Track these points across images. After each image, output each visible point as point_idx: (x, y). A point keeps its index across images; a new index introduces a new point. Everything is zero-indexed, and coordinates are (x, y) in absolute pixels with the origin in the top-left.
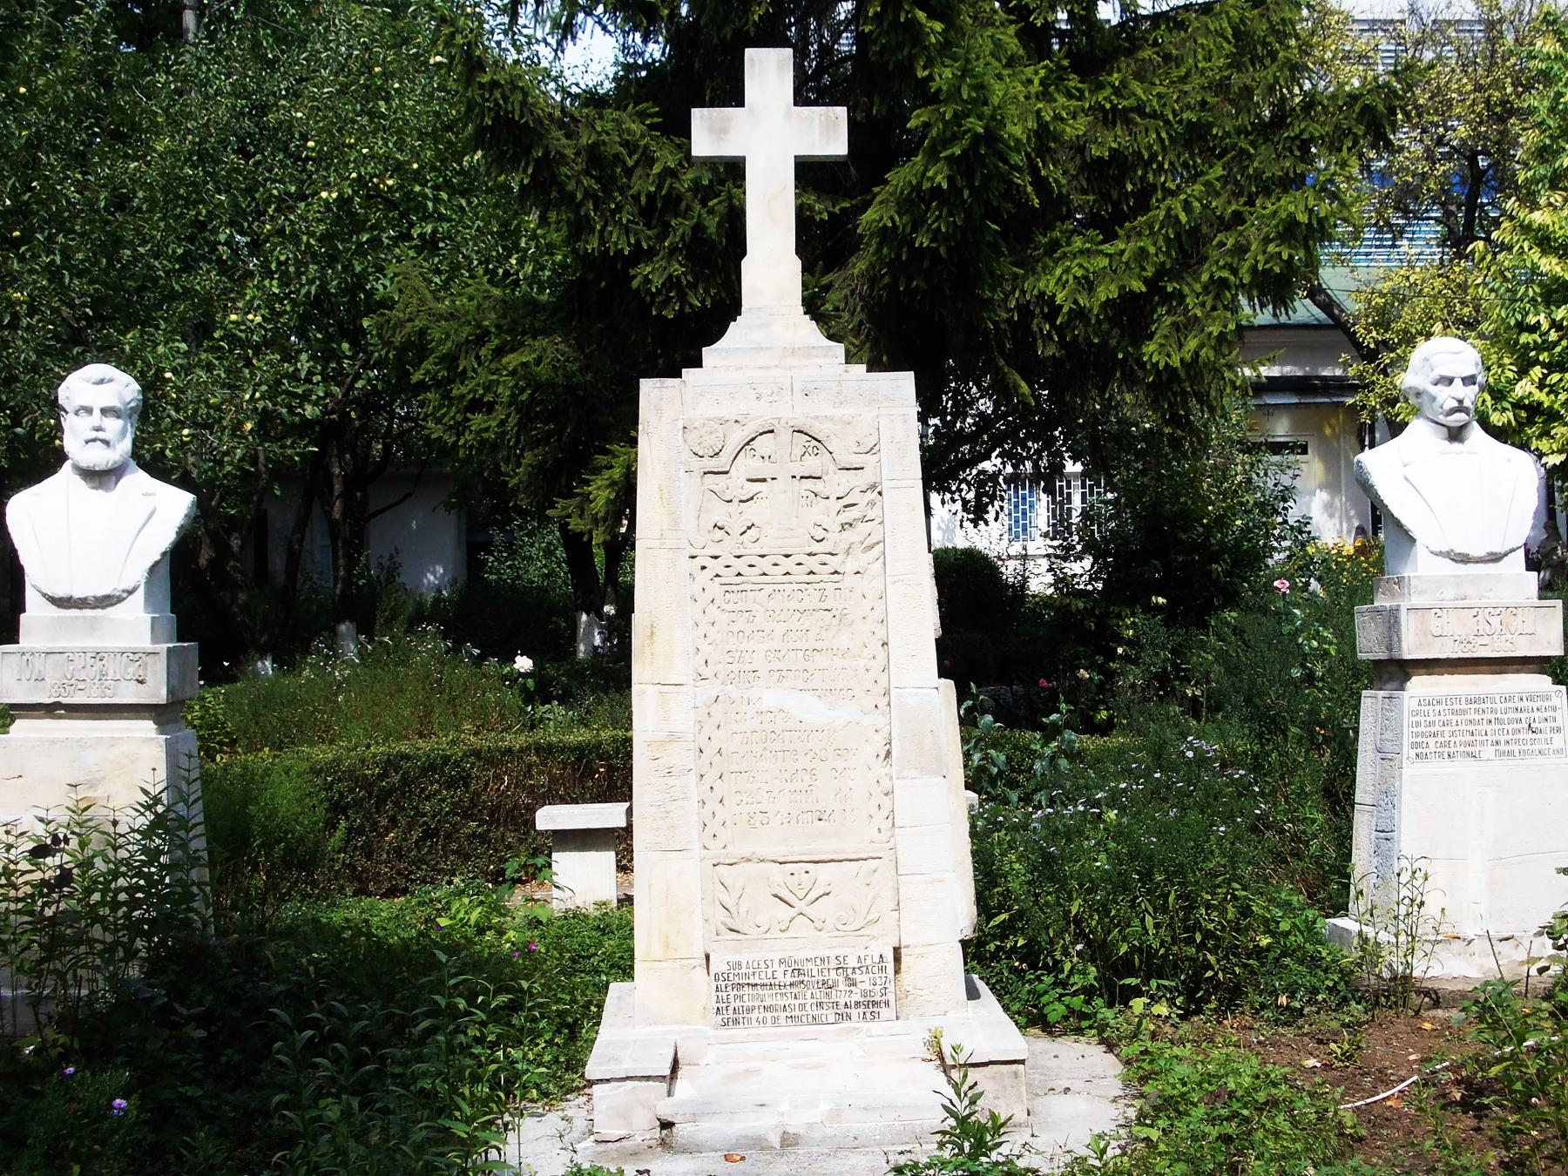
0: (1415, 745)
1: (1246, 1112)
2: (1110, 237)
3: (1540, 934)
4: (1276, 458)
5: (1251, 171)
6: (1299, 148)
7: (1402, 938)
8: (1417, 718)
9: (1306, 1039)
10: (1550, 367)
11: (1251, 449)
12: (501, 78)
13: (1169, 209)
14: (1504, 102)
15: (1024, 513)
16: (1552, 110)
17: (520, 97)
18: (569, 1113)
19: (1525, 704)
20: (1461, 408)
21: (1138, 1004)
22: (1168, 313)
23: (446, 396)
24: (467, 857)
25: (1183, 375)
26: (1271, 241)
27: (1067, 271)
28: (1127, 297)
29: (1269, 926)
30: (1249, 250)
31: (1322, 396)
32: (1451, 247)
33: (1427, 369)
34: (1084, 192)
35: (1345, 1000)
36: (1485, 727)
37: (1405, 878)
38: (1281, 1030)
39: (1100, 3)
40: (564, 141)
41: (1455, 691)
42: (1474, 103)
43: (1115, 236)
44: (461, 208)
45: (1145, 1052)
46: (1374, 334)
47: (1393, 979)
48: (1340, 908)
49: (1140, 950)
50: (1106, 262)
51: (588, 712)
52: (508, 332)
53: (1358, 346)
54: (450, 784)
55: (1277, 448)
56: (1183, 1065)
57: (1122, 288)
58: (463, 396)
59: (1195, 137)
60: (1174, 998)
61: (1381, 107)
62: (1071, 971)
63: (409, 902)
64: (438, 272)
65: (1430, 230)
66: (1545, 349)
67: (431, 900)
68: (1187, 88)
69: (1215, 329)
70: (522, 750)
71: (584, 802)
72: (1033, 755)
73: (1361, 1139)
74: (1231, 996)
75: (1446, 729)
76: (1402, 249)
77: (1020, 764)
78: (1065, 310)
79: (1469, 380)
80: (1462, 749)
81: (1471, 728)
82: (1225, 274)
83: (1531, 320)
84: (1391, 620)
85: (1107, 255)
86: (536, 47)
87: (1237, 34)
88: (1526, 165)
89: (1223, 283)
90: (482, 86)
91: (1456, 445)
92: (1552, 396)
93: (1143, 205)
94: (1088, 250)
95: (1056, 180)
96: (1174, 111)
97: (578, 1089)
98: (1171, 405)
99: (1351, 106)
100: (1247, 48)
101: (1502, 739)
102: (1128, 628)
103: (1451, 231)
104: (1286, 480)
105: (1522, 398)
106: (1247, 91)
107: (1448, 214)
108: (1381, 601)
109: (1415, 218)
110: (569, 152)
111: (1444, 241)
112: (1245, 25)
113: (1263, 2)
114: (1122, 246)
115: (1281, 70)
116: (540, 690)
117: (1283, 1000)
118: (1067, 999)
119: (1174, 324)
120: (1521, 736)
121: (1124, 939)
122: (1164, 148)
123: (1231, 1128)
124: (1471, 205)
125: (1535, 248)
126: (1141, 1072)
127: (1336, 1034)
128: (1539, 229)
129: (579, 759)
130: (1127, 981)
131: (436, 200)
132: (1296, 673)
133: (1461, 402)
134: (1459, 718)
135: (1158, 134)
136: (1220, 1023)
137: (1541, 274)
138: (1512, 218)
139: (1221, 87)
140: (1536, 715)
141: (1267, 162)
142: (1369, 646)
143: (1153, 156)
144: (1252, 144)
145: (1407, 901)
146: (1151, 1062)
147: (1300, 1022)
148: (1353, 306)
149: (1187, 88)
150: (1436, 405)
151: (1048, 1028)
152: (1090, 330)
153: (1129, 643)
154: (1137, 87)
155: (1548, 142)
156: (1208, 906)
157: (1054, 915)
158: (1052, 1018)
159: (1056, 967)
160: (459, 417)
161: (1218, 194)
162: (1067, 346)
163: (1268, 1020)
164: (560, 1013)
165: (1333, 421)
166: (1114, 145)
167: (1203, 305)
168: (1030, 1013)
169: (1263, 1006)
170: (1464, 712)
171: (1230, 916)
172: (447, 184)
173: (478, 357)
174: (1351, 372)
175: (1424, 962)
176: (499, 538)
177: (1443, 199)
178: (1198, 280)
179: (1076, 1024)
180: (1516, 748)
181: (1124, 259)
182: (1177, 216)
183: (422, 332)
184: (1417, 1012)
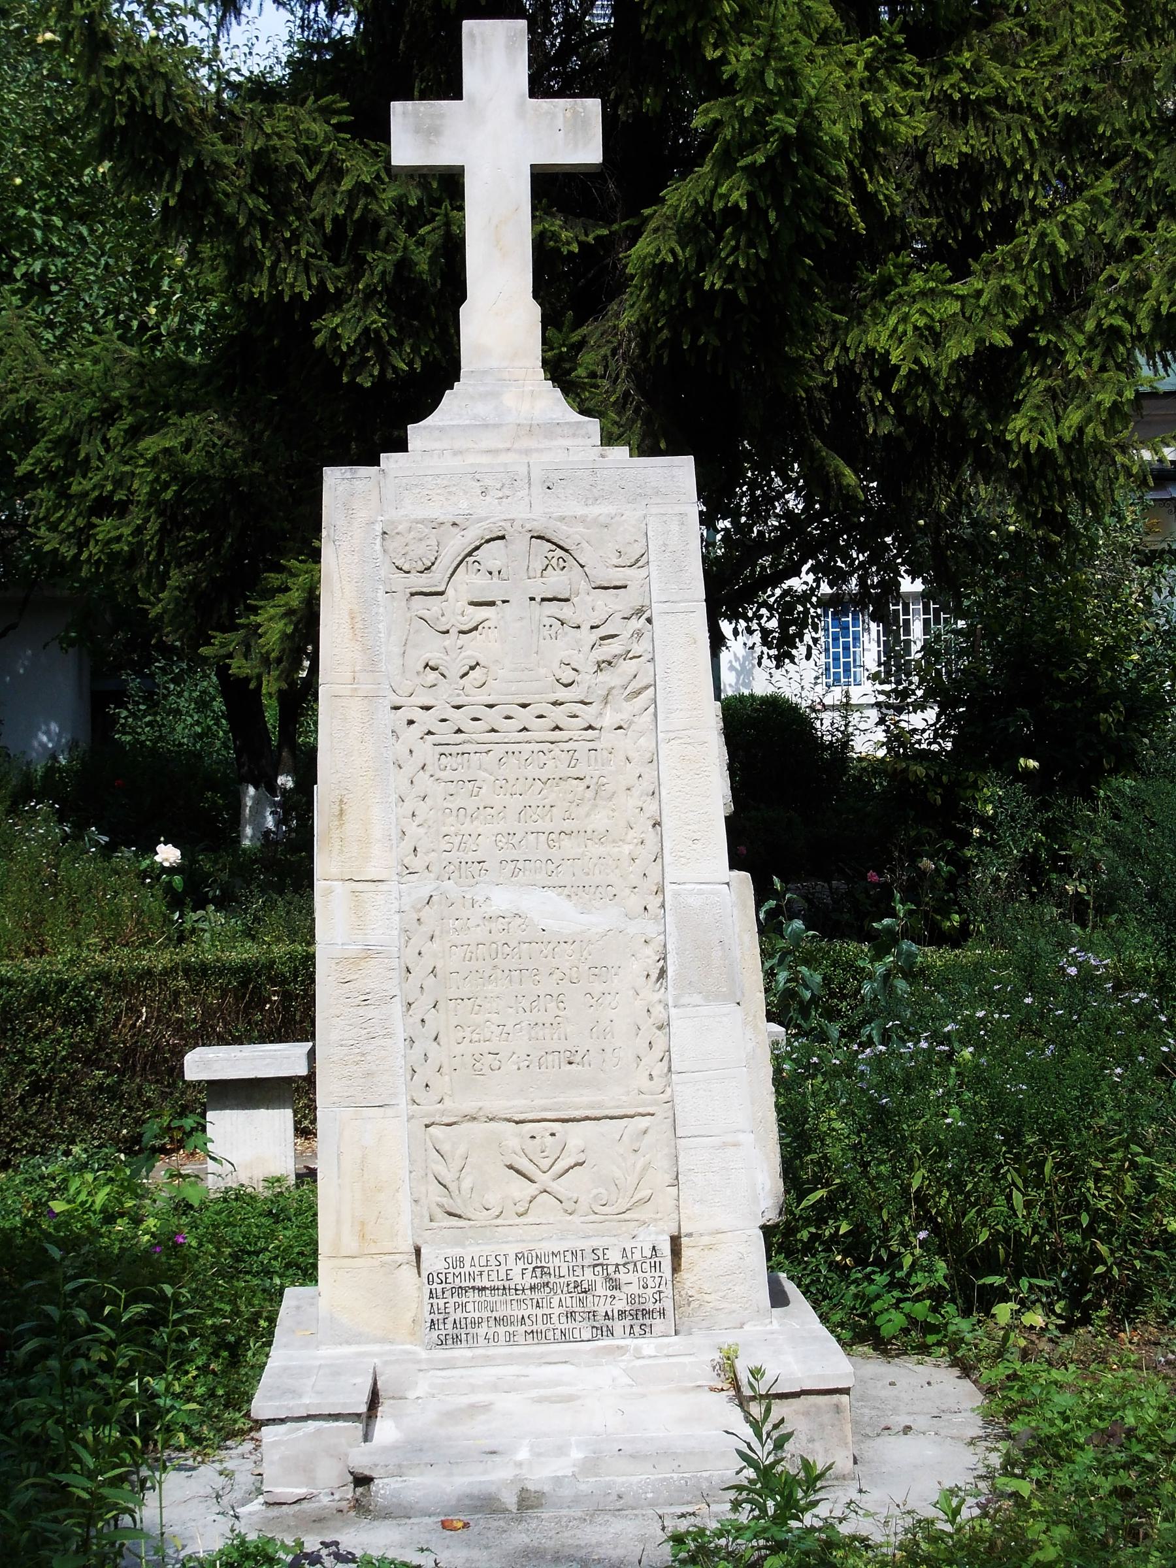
1: (1149, 1457)
2: (961, 273)
5: (1150, 183)
12: (136, 60)
13: (1043, 235)
15: (846, 648)
17: (162, 87)
18: (229, 1465)
21: (1003, 1311)
22: (1041, 374)
23: (63, 492)
24: (90, 1118)
27: (905, 319)
28: (987, 355)
34: (925, 213)
40: (221, 146)
44: (81, 237)
49: (1006, 1239)
50: (956, 307)
51: (257, 919)
52: (147, 405)
54: (68, 1019)
56: (1065, 1393)
57: (980, 341)
58: (85, 494)
59: (1075, 136)
60: (1052, 1304)
63: (10, 1179)
64: (50, 325)
67: (42, 1177)
68: (1061, 71)
69: (1106, 398)
70: (166, 972)
71: (251, 1041)
74: (1130, 1302)
78: (903, 371)
82: (1118, 321)
85: (958, 297)
86: (181, 20)
89: (1115, 333)
90: (109, 72)
94: (932, 290)
95: (887, 198)
96: (1045, 101)
97: (242, 1432)
102: (986, 801)
110: (229, 161)
114: (979, 285)
116: (190, 890)
118: (907, 1306)
119: (1049, 389)
122: (1032, 153)
123: (1129, 1479)
129: (244, 984)
131: (48, 227)
135: (1025, 135)
136: (1114, 1336)
139: (1107, 69)
144: (1150, 146)
146: (1021, 1390)
149: (1061, 71)
154: (995, 71)
156: (1098, 1177)
158: (887, 1331)
159: (894, 1261)
160: (81, 522)
164: (217, 1330)
167: (1088, 363)
168: (856, 1325)
171: (1129, 1190)
172: (62, 207)
173: (105, 440)
176: (134, 684)
178: (1080, 329)
179: (919, 1340)
181: (982, 302)
183: (30, 407)
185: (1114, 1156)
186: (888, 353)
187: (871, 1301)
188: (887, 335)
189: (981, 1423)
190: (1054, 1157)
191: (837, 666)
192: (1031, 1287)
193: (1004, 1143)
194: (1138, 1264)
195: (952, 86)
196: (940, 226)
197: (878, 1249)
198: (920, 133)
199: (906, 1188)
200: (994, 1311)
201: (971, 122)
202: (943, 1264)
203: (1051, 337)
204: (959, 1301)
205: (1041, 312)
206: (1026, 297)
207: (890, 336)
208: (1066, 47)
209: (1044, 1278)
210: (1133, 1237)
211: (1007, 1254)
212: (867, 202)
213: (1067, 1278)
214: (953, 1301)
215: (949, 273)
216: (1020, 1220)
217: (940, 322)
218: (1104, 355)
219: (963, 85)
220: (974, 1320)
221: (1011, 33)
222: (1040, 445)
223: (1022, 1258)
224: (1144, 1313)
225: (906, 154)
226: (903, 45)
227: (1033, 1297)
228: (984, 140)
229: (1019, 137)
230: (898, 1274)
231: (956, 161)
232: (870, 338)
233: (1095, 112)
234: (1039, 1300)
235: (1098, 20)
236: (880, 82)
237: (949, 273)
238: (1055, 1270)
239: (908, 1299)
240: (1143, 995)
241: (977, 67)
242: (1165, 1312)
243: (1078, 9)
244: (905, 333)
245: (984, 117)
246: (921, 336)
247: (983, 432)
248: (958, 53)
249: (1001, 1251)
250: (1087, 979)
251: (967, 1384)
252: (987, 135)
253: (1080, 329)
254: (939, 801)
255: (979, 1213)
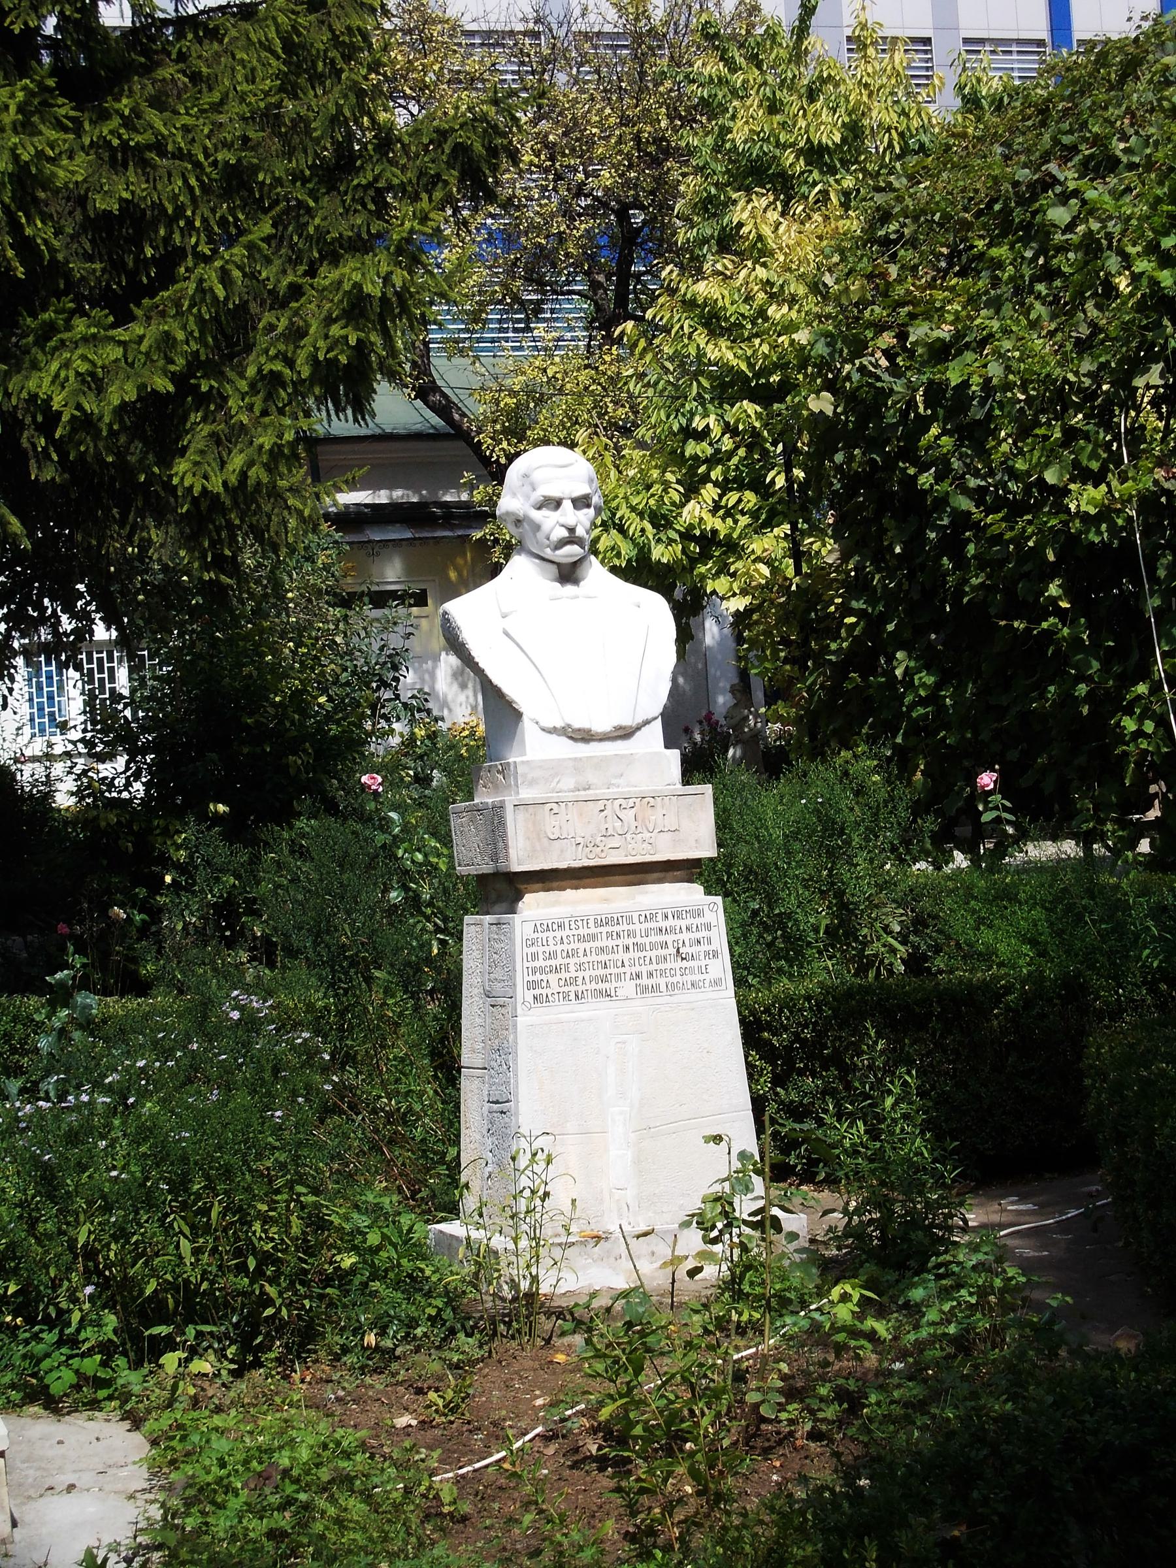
0: (532, 985)
1: (303, 1497)
2: (124, 319)
3: (686, 1225)
4: (377, 613)
5: (311, 230)
6: (373, 201)
7: (524, 1243)
8: (534, 949)
9: (401, 1389)
10: (724, 486)
11: (347, 601)
13: (201, 281)
14: (658, 140)
15: (51, 698)
16: (717, 148)
19: (671, 922)
20: (572, 538)
21: (171, 1360)
22: (204, 419)
25: (228, 502)
26: (335, 321)
27: (66, 365)
28: (150, 398)
29: (352, 1240)
30: (306, 334)
31: (443, 527)
32: (599, 329)
33: (527, 488)
34: (90, 258)
35: (452, 1332)
36: (621, 955)
37: (523, 1161)
38: (368, 1380)
39: (100, 4)
41: (582, 909)
42: (620, 141)
43: (132, 318)
45: (180, 1427)
46: (505, 445)
47: (515, 1299)
48: (452, 1210)
49: (173, 1287)
50: (118, 352)
53: (486, 461)
55: (380, 599)
56: (226, 1437)
57: (141, 387)
59: (237, 182)
60: (224, 1349)
61: (478, 147)
62: (82, 1320)
65: (575, 308)
66: (719, 462)
68: (222, 119)
69: (266, 440)
72: (39, 1027)
73: (464, 1519)
74: (303, 1339)
75: (572, 961)
76: (536, 333)
77: (23, 1041)
78: (65, 418)
79: (581, 502)
80: (594, 986)
81: (603, 958)
82: (278, 366)
83: (698, 423)
84: (495, 819)
85: (120, 343)
87: (288, 46)
88: (687, 219)
89: (275, 379)
91: (570, 589)
92: (729, 521)
93: (167, 277)
94: (94, 336)
95: (46, 242)
96: (205, 149)
98: (213, 544)
99: (439, 145)
100: (300, 65)
101: (644, 970)
102: (178, 847)
103: (599, 308)
104: (395, 641)
105: (691, 527)
106: (300, 121)
107: (595, 286)
108: (483, 797)
109: (554, 292)
111: (591, 323)
112: (299, 35)
113: (324, 4)
114: (140, 331)
115: (345, 96)
117: (371, 1339)
118: (75, 1362)
119: (213, 435)
120: (668, 965)
121: (154, 1273)
122: (194, 199)
123: (285, 1520)
124: (624, 275)
125: (700, 329)
126: (171, 1449)
127: (441, 1378)
128: (705, 304)
130: (156, 1330)
132: (395, 896)
133: (572, 530)
134: (587, 945)
135: (186, 181)
136: (286, 1377)
137: (710, 364)
138: (672, 292)
139: (269, 118)
140: (686, 936)
141: (331, 217)
142: (471, 859)
143: (180, 210)
144: (312, 194)
145: (527, 1193)
146: (183, 1439)
147: (394, 1366)
148: (477, 409)
149: (222, 119)
150: (540, 536)
151: (53, 1405)
152: (101, 445)
153: (181, 868)
154: (154, 117)
155: (713, 191)
156: (266, 1220)
157: (58, 1248)
158: (56, 1389)
159: (62, 1318)
161: (268, 261)
162: (73, 467)
163: (352, 1368)
165: (460, 561)
166: (126, 195)
167: (250, 408)
168: (27, 1385)
169: (345, 1350)
170: (593, 937)
171: (295, 1230)
174: (477, 497)
175: (553, 1272)
177: (588, 263)
178: (242, 375)
179: (90, 1395)
180: (662, 982)
181: (143, 348)
182: (211, 289)
184: (548, 1341)
185: (279, 1197)
186: (50, 398)
187: (39, 1361)
188: (50, 381)
189: (146, 1476)
190: (220, 1202)
191: (41, 716)
192: (199, 1335)
193: (169, 1191)
194: (307, 1303)
195: (111, 132)
196: (103, 270)
197: (46, 1307)
198: (80, 178)
199: (73, 1242)
200: (161, 1361)
201: (131, 168)
202: (113, 1317)
203: (213, 383)
204: (132, 1355)
205: (203, 358)
206: (187, 343)
207: (53, 382)
208: (227, 94)
209: (215, 1324)
210: (301, 1276)
211: (177, 1303)
212: (26, 247)
213: (239, 1322)
214: (125, 1354)
215: (111, 319)
216: (189, 1268)
217: (103, 368)
218: (265, 400)
219: (122, 131)
220: (145, 1371)
221: (173, 79)
222: (204, 487)
223: (192, 1305)
224: (315, 1352)
225: (68, 199)
226: (54, 89)
227: (205, 1344)
228: (144, 186)
229: (180, 183)
230: (68, 1331)
231: (117, 206)
232: (32, 384)
233: (255, 161)
234: (210, 1347)
235: (259, 67)
236: (33, 125)
237: (111, 319)
238: (225, 1316)
239: (77, 1355)
240: (306, 1035)
241: (136, 112)
242: (337, 1349)
243: (238, 57)
244: (67, 379)
245: (144, 164)
246: (84, 382)
247: (150, 475)
248: (118, 100)
249: (170, 1301)
250: (251, 1022)
251: (138, 1438)
252: (147, 181)
253: (242, 375)
254: (131, 849)
255: (146, 1264)
